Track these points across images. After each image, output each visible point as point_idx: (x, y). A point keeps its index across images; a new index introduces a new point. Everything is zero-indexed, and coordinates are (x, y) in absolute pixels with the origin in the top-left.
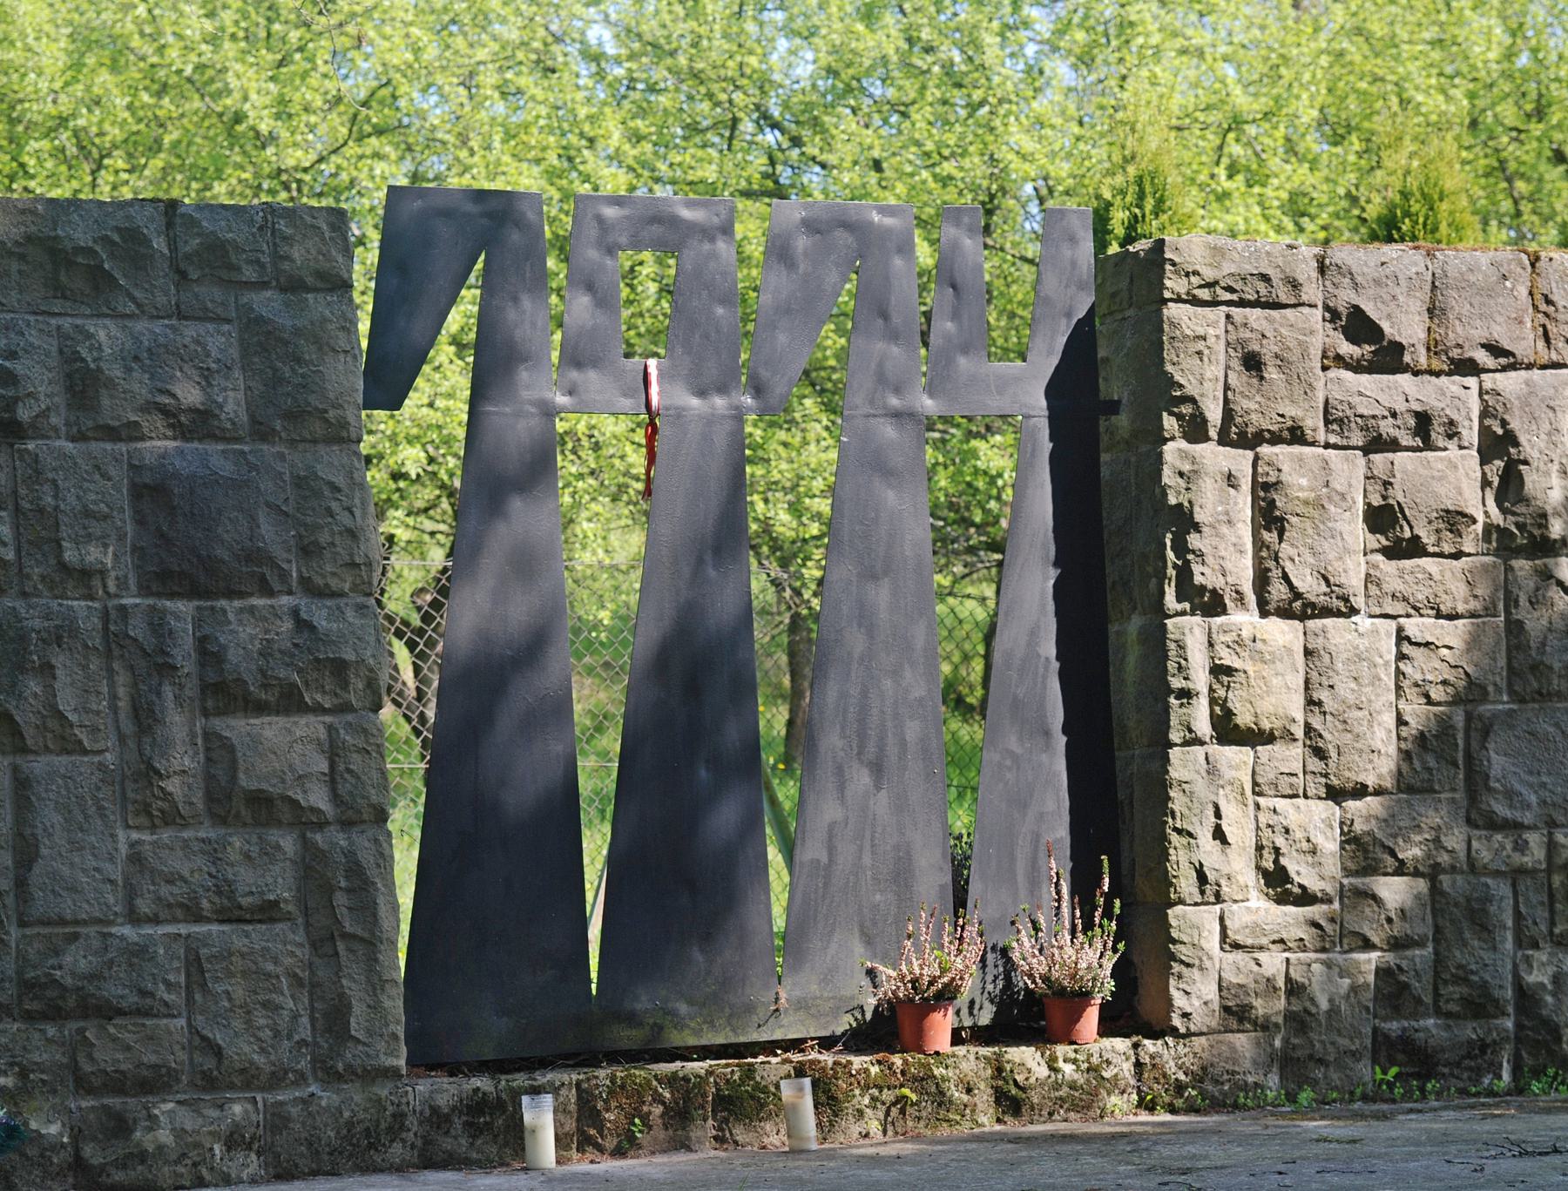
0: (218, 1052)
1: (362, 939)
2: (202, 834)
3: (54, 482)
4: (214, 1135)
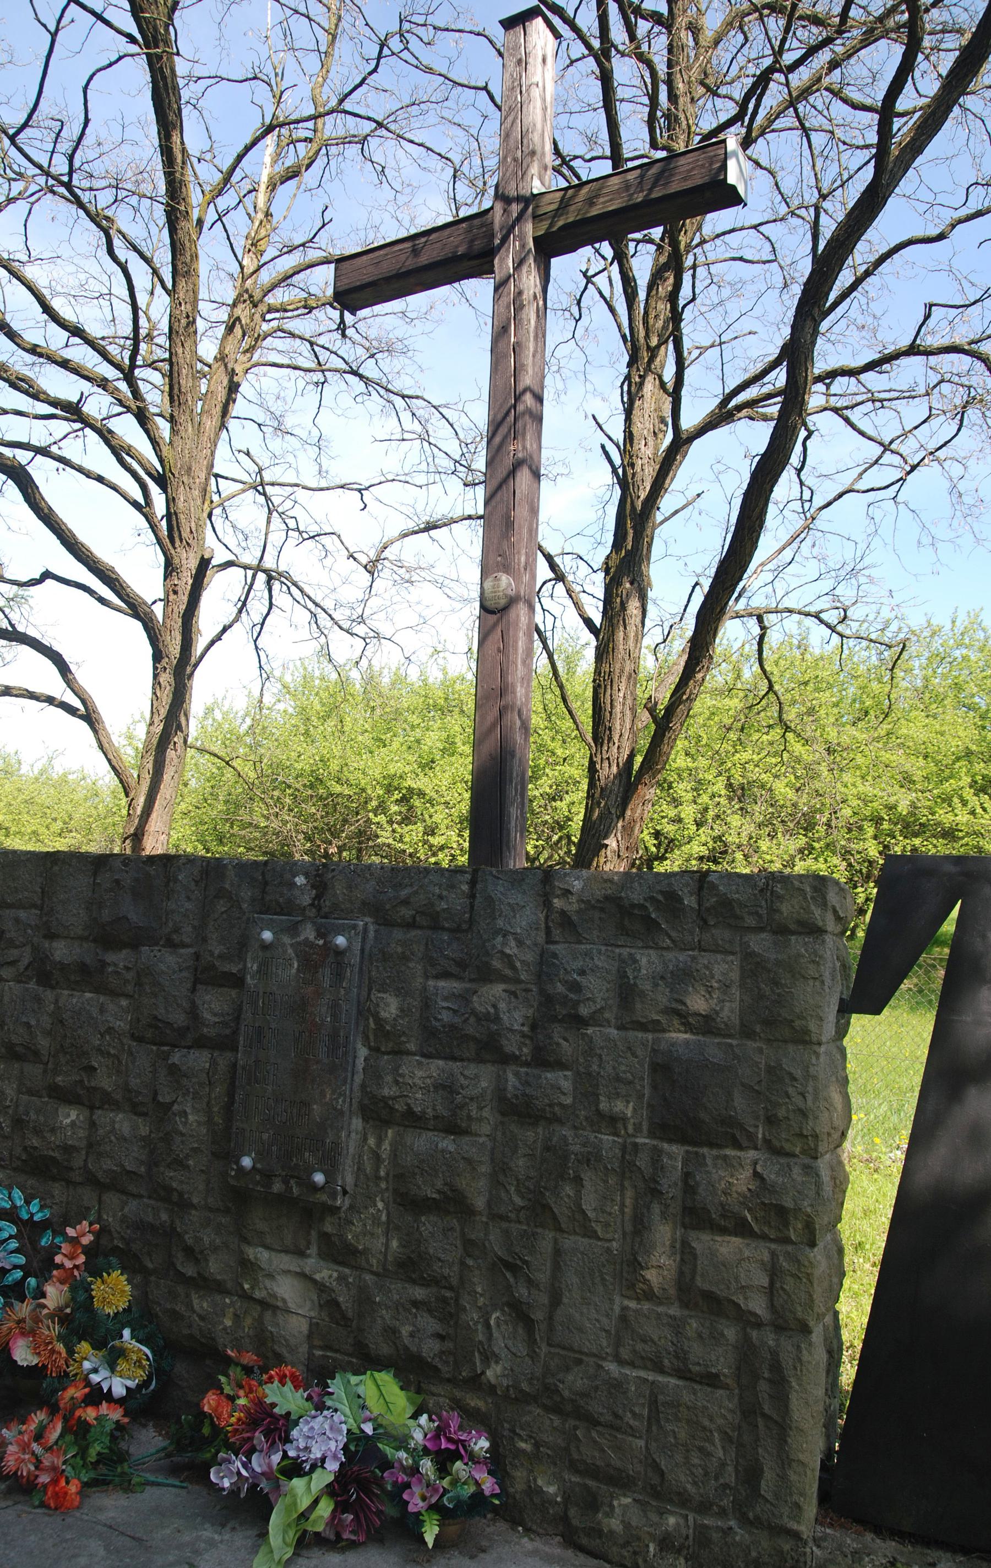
0: (662, 1474)
1: (776, 1422)
2: (671, 1312)
3: (600, 1056)
4: (652, 1537)
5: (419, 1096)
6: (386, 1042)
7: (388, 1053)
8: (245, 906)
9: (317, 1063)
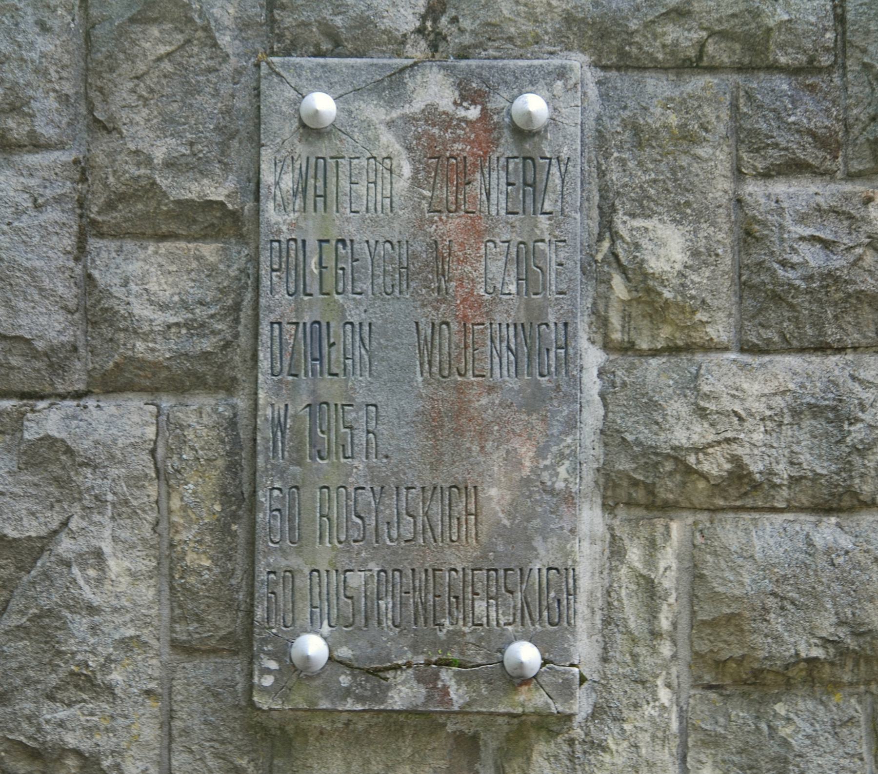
5: (758, 437)
6: (656, 326)
7: (655, 353)
8: (225, 40)
9: (491, 389)
